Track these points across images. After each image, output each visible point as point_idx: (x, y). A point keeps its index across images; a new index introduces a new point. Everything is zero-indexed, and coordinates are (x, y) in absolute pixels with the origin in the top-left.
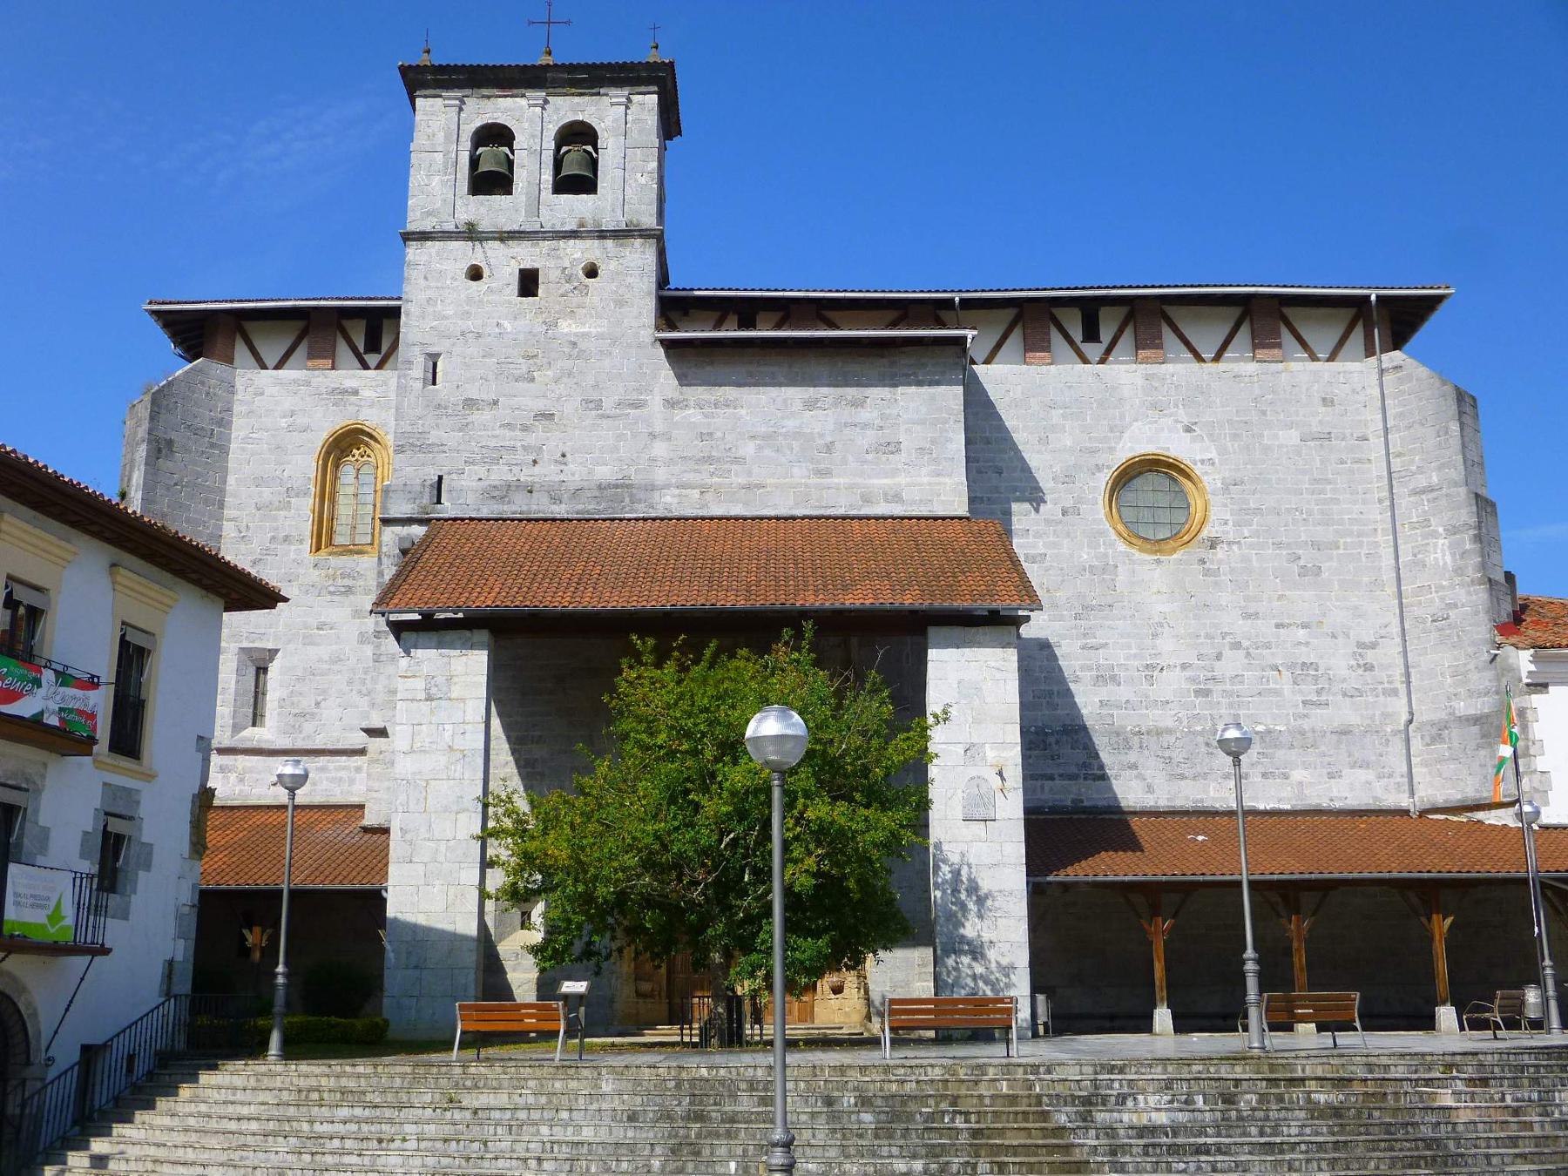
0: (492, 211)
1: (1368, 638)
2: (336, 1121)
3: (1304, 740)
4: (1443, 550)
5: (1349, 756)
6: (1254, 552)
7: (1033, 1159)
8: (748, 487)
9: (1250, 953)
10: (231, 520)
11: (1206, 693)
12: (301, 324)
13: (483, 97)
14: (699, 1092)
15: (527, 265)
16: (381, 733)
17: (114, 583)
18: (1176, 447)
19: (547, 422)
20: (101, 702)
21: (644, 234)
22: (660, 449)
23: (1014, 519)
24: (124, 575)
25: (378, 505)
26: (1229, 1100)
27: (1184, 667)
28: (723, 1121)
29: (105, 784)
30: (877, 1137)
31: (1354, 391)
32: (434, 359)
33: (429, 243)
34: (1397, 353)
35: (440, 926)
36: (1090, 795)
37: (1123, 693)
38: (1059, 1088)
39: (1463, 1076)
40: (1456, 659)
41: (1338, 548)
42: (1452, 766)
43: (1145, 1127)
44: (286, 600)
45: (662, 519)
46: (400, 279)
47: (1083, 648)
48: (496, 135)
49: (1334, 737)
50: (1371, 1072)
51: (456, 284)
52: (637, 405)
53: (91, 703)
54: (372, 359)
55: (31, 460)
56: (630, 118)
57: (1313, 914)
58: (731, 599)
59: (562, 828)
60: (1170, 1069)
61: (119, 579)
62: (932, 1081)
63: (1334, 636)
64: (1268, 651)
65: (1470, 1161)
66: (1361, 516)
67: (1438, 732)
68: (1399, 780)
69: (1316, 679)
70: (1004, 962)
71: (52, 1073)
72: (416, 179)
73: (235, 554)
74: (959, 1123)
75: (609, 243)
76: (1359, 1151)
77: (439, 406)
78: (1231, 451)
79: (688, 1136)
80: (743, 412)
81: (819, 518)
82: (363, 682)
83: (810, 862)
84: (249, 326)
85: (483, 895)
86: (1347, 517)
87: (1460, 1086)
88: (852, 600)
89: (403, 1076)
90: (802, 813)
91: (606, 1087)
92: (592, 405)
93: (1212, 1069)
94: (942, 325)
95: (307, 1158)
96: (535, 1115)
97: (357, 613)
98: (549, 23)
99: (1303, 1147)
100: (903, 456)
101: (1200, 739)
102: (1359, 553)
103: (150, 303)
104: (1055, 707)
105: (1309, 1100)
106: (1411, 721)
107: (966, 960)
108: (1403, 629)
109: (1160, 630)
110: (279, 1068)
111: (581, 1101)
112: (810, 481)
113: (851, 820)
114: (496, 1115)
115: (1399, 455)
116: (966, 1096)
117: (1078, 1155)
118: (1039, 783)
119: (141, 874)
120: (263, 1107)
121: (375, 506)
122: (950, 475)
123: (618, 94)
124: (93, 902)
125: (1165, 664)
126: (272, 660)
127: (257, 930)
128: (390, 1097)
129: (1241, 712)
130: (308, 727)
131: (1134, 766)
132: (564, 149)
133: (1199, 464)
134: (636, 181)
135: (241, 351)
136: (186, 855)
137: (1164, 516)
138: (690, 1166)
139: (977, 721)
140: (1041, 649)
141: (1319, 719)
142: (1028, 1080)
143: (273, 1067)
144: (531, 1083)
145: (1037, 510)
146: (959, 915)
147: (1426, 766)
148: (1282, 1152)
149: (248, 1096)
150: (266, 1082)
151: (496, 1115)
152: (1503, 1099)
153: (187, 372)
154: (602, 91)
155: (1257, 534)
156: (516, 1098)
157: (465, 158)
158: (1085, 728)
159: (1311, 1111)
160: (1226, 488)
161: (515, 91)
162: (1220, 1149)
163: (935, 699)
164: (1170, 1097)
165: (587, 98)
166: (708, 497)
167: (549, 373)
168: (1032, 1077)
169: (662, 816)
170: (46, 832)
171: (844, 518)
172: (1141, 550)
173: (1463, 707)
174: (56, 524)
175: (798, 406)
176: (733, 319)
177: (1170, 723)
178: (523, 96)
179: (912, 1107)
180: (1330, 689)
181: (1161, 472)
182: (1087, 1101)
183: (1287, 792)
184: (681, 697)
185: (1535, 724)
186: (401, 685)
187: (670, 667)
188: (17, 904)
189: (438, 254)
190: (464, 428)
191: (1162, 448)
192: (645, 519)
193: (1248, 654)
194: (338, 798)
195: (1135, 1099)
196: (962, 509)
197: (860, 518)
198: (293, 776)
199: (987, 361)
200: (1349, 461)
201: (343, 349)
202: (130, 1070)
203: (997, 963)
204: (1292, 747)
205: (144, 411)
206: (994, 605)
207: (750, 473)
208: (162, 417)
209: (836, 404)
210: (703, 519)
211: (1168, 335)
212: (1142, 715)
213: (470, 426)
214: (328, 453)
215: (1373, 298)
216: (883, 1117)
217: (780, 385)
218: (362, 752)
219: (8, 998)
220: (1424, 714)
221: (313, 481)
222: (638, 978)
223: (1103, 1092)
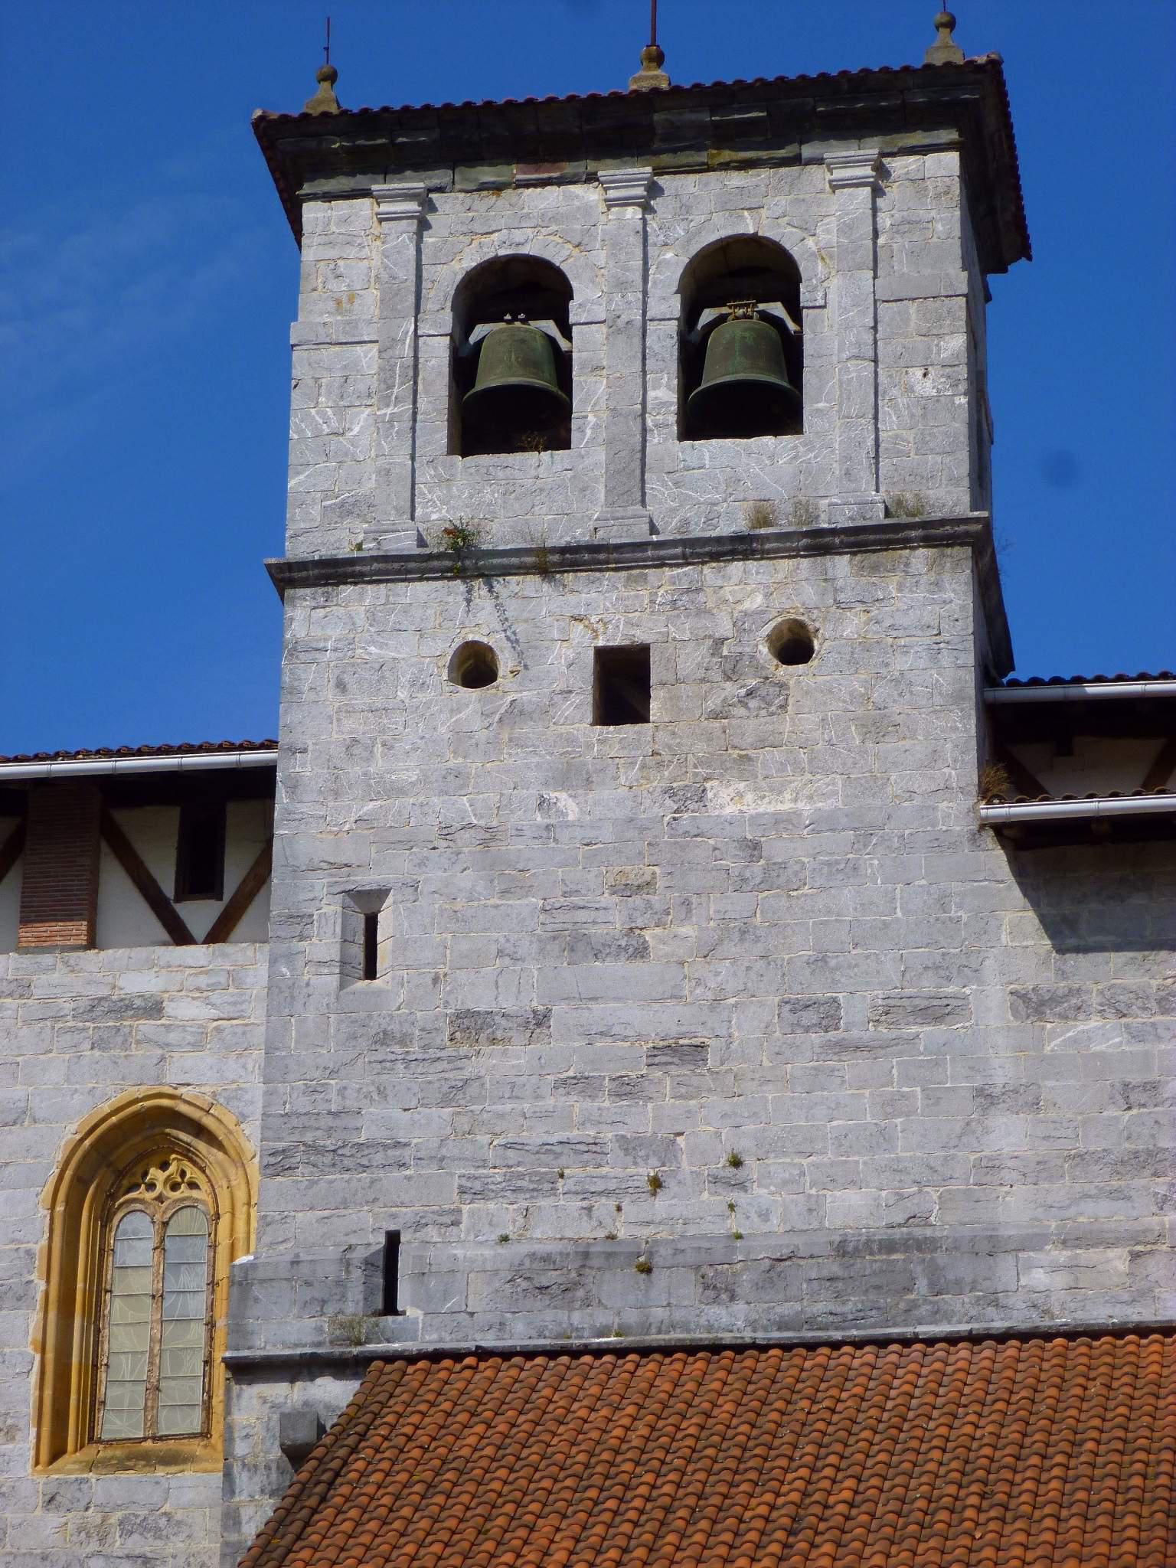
13: (483, 187)
15: (616, 637)
33: (347, 591)
51: (422, 697)
52: (936, 1012)
56: (885, 221)
75: (841, 565)
77: (384, 1038)
92: (810, 1017)
134: (909, 389)
154: (807, 151)
165: (765, 174)
190: (454, 1094)
213: (473, 1089)
214: (80, 1183)
221: (40, 1263)
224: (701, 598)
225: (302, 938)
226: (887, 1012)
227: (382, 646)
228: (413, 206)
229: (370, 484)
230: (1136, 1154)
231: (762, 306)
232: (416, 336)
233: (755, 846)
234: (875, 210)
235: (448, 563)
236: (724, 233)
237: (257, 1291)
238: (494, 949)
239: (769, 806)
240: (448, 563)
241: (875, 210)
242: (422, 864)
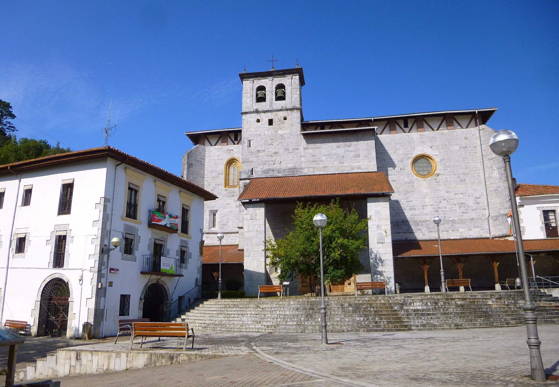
0: (261, 106)
1: (478, 196)
2: (233, 311)
3: (462, 222)
4: (496, 174)
5: (474, 225)
6: (448, 176)
7: (389, 317)
8: (324, 167)
9: (442, 270)
10: (206, 181)
11: (437, 211)
12: (219, 135)
14: (312, 304)
16: (242, 228)
17: (180, 195)
19: (276, 154)
20: (179, 221)
21: (297, 109)
22: (303, 159)
23: (389, 171)
24: (182, 194)
25: (239, 176)
26: (436, 303)
27: (432, 205)
28: (318, 310)
29: (181, 240)
30: (353, 313)
31: (473, 135)
32: (250, 141)
34: (483, 125)
35: (256, 271)
36: (410, 237)
37: (417, 212)
38: (396, 302)
39: (494, 297)
40: (500, 200)
42: (500, 226)
43: (415, 310)
44: (218, 198)
45: (304, 176)
46: (241, 123)
48: (261, 88)
49: (470, 220)
50: (472, 297)
52: (297, 149)
53: (177, 222)
54: (236, 142)
55: (161, 169)
56: (292, 82)
57: (464, 263)
58: (320, 193)
59: (282, 247)
60: (422, 297)
61: (181, 194)
62: (366, 300)
63: (469, 196)
65: (494, 316)
66: (476, 166)
67: (496, 218)
68: (486, 230)
69: (465, 207)
70: (388, 276)
71: (173, 302)
72: (244, 100)
73: (207, 188)
74: (372, 309)
76: (467, 314)
79: (310, 313)
80: (322, 149)
81: (341, 173)
82: (237, 216)
83: (339, 252)
84: (208, 136)
85: (266, 265)
87: (494, 300)
88: (350, 192)
89: (247, 302)
90: (337, 241)
91: (292, 303)
92: (287, 150)
93: (432, 297)
94: (369, 126)
95: (227, 319)
96: (276, 309)
97: (235, 201)
99: (453, 313)
100: (361, 158)
104: (400, 216)
105: (456, 303)
106: (489, 216)
107: (379, 276)
108: (487, 193)
109: (425, 196)
110: (221, 300)
111: (286, 306)
112: (339, 165)
113: (348, 243)
114: (267, 309)
115: (485, 150)
116: (374, 303)
117: (399, 316)
118: (397, 234)
119: (190, 260)
120: (217, 308)
121: (238, 176)
122: (372, 162)
123: (289, 77)
124: (179, 265)
126: (217, 212)
127: (216, 273)
128: (244, 306)
130: (225, 228)
131: (420, 230)
132: (277, 90)
135: (206, 142)
136: (199, 255)
137: (425, 169)
138: (310, 319)
139: (380, 220)
141: (466, 216)
142: (388, 300)
143: (219, 300)
144: (275, 303)
145: (394, 169)
146: (377, 265)
147: (494, 227)
148: (448, 315)
149: (214, 306)
150: (218, 303)
151: (267, 309)
152: (505, 302)
153: (195, 148)
154: (286, 76)
155: (449, 172)
156: (272, 306)
157: (274, 93)
158: (407, 221)
159: (456, 306)
160: (441, 161)
161: (266, 78)
162: (433, 314)
163: (369, 214)
164: (422, 303)
165: (282, 78)
166: (315, 170)
167: (277, 143)
168: (389, 299)
169: (305, 244)
170: (169, 250)
171: (347, 173)
172: (420, 177)
173: (502, 212)
174: (167, 183)
175: (335, 147)
176: (319, 128)
177: (429, 219)
178: (267, 78)
179: (361, 306)
182: (402, 304)
183: (458, 234)
184: (309, 217)
185: (521, 215)
186: (245, 216)
187: (306, 210)
188: (163, 265)
189: (249, 117)
191: (425, 153)
192: (300, 176)
193: (448, 201)
194: (233, 243)
195: (413, 304)
196: (376, 170)
197: (351, 173)
198: (221, 236)
199: (381, 134)
201: (229, 140)
202: (189, 302)
203: (387, 276)
204: (459, 223)
205: (186, 157)
206: (384, 192)
208: (190, 158)
210: (314, 175)
211: (425, 125)
212: (422, 217)
214: (227, 165)
215: (477, 112)
216: (354, 308)
217: (331, 143)
218: (238, 233)
219: (163, 286)
220: (493, 214)
221: (224, 171)
222: (303, 283)
223: (406, 302)
226: (293, 149)
237: (241, 173)
242: (254, 138)
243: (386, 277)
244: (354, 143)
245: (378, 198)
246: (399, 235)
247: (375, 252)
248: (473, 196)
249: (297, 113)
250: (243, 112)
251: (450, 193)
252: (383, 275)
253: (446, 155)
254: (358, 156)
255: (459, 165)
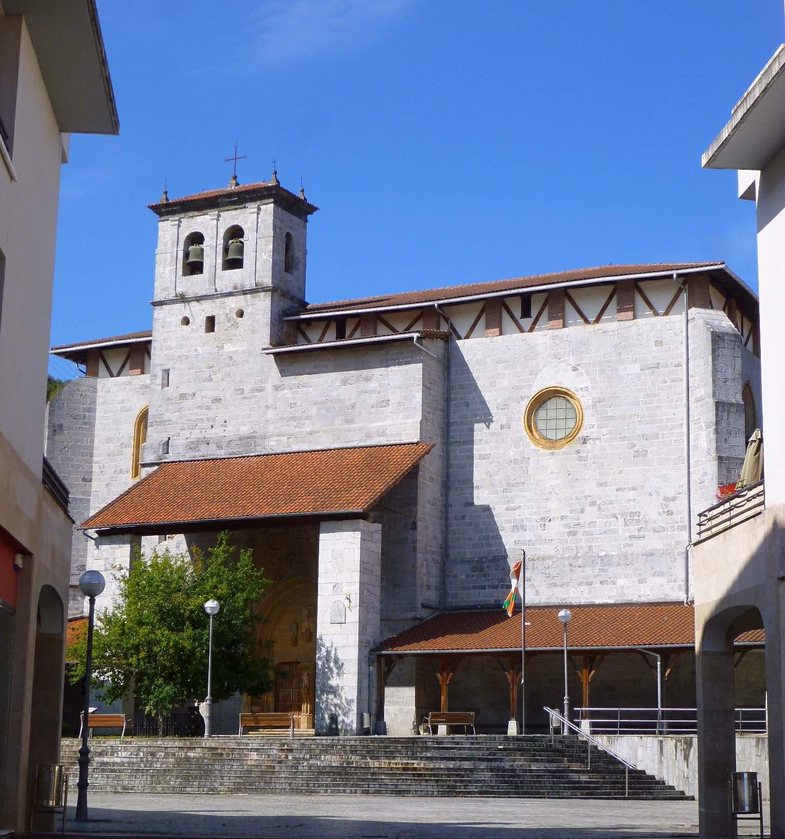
1: (670, 494)
3: (626, 560)
5: (652, 569)
8: (310, 434)
11: (574, 534)
13: (190, 217)
18: (567, 381)
21: (265, 290)
22: (271, 414)
27: (563, 518)
32: (167, 372)
33: (164, 306)
37: (528, 535)
41: (658, 438)
47: (507, 509)
51: (177, 328)
52: (260, 390)
56: (260, 220)
63: (650, 494)
64: (611, 506)
68: (681, 583)
69: (638, 521)
72: (159, 269)
75: (249, 296)
77: (168, 399)
78: (599, 381)
80: (311, 389)
86: (664, 417)
92: (239, 392)
98: (236, 159)
99: (151, 771)
100: (390, 409)
101: (566, 562)
102: (671, 440)
103: (52, 350)
104: (488, 545)
107: (331, 696)
123: (252, 207)
125: (552, 517)
129: (593, 544)
133: (579, 391)
134: (262, 258)
140: (484, 512)
141: (639, 546)
145: (488, 427)
160: (594, 406)
164: (130, 753)
165: (239, 210)
166: (291, 440)
175: (338, 383)
177: (553, 553)
180: (646, 527)
181: (562, 397)
183: (614, 592)
190: (179, 410)
193: (600, 508)
195: (117, 753)
200: (668, 381)
204: (619, 565)
207: (314, 424)
209: (357, 381)
213: (183, 409)
221: (133, 439)
224: (224, 305)
225: (155, 379)
226: (252, 390)
227: (170, 318)
228: (177, 222)
229: (168, 284)
230: (292, 417)
231: (240, 239)
232: (177, 251)
233: (231, 357)
234: (258, 218)
235: (180, 300)
236: (232, 225)
237: (146, 450)
238: (187, 381)
239: (234, 349)
240: (180, 300)
241: (258, 218)
242: (175, 363)
243: (344, 698)
244: (378, 372)
245: (340, 523)
246: (481, 594)
247: (328, 644)
248: (658, 493)
249: (265, 300)
250: (155, 300)
251: (607, 488)
252: (339, 695)
253: (606, 388)
254: (384, 404)
255: (635, 415)
